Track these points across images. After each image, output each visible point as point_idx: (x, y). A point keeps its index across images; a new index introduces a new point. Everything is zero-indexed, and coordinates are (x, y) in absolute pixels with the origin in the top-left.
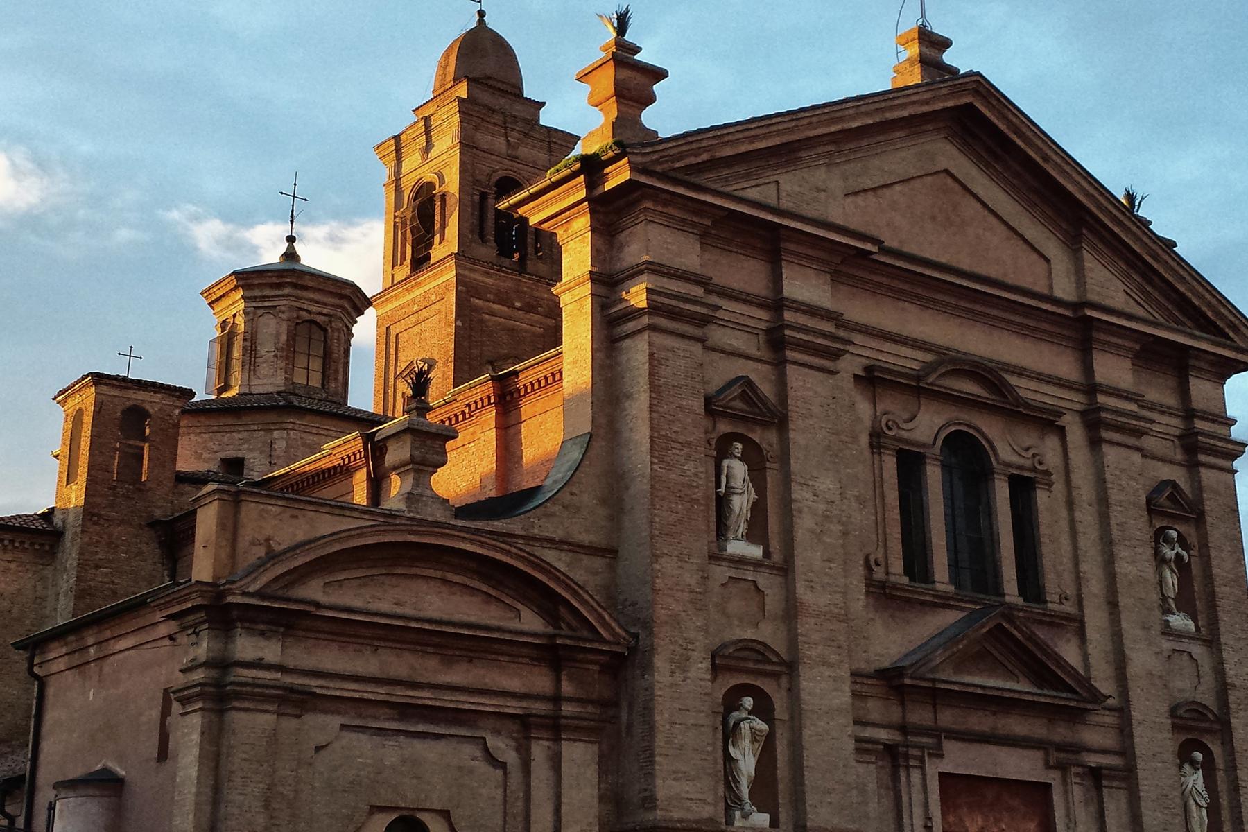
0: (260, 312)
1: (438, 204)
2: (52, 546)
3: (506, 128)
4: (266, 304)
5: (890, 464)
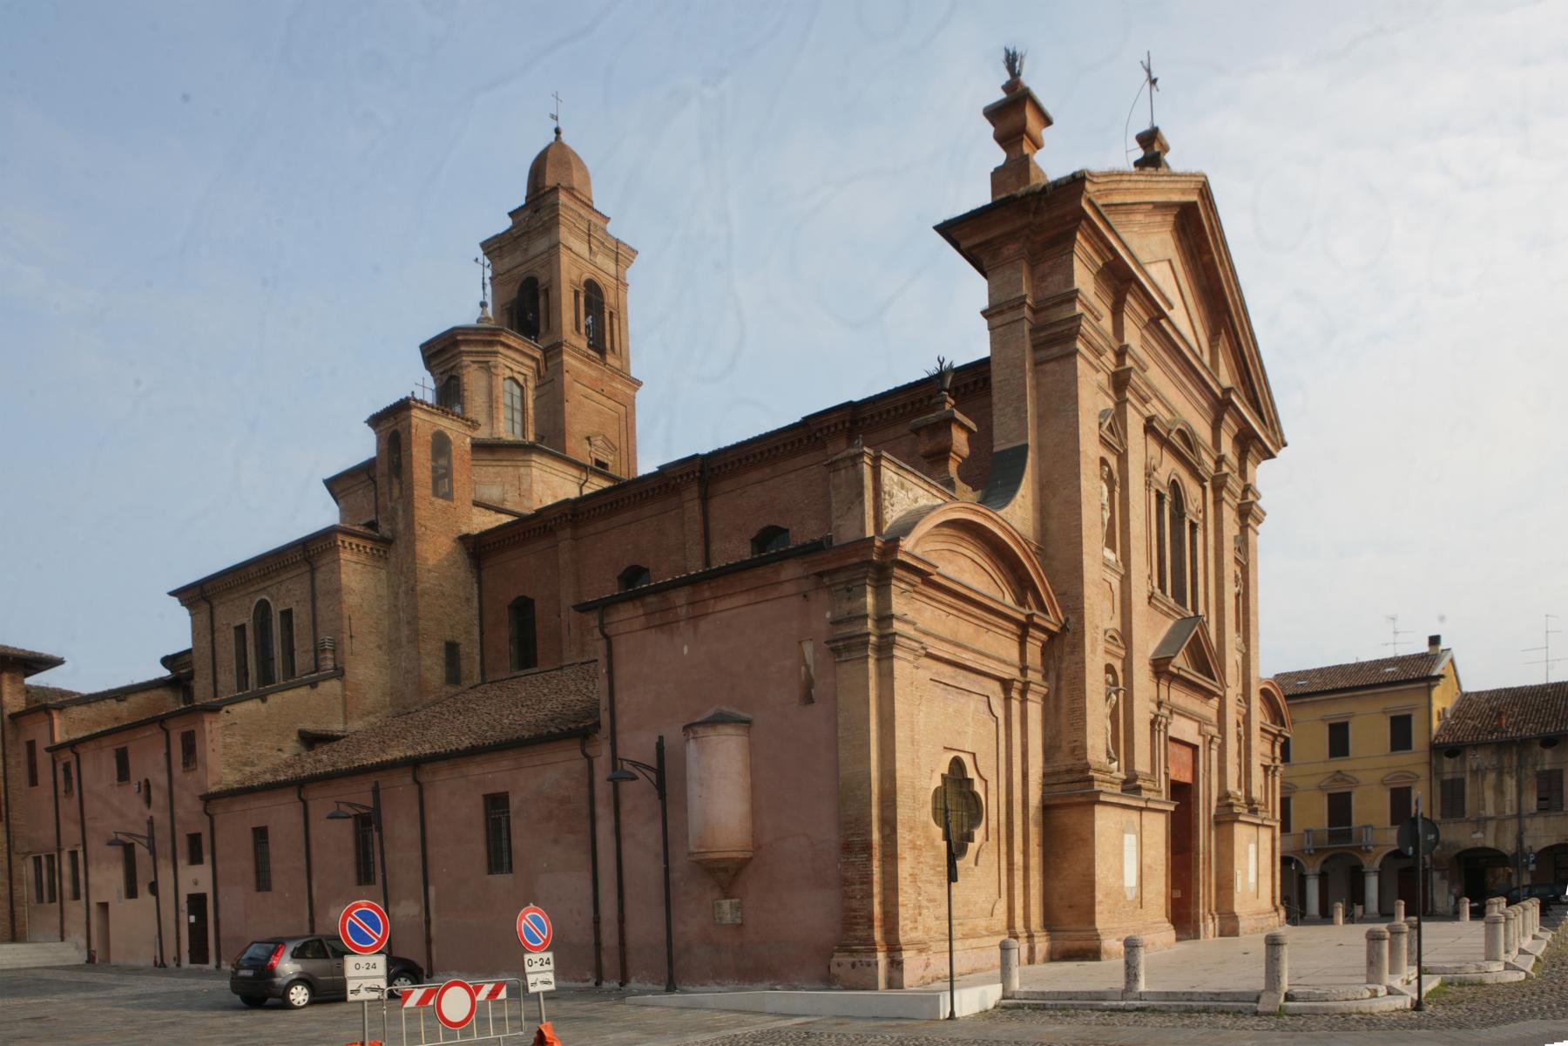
5: (1153, 495)
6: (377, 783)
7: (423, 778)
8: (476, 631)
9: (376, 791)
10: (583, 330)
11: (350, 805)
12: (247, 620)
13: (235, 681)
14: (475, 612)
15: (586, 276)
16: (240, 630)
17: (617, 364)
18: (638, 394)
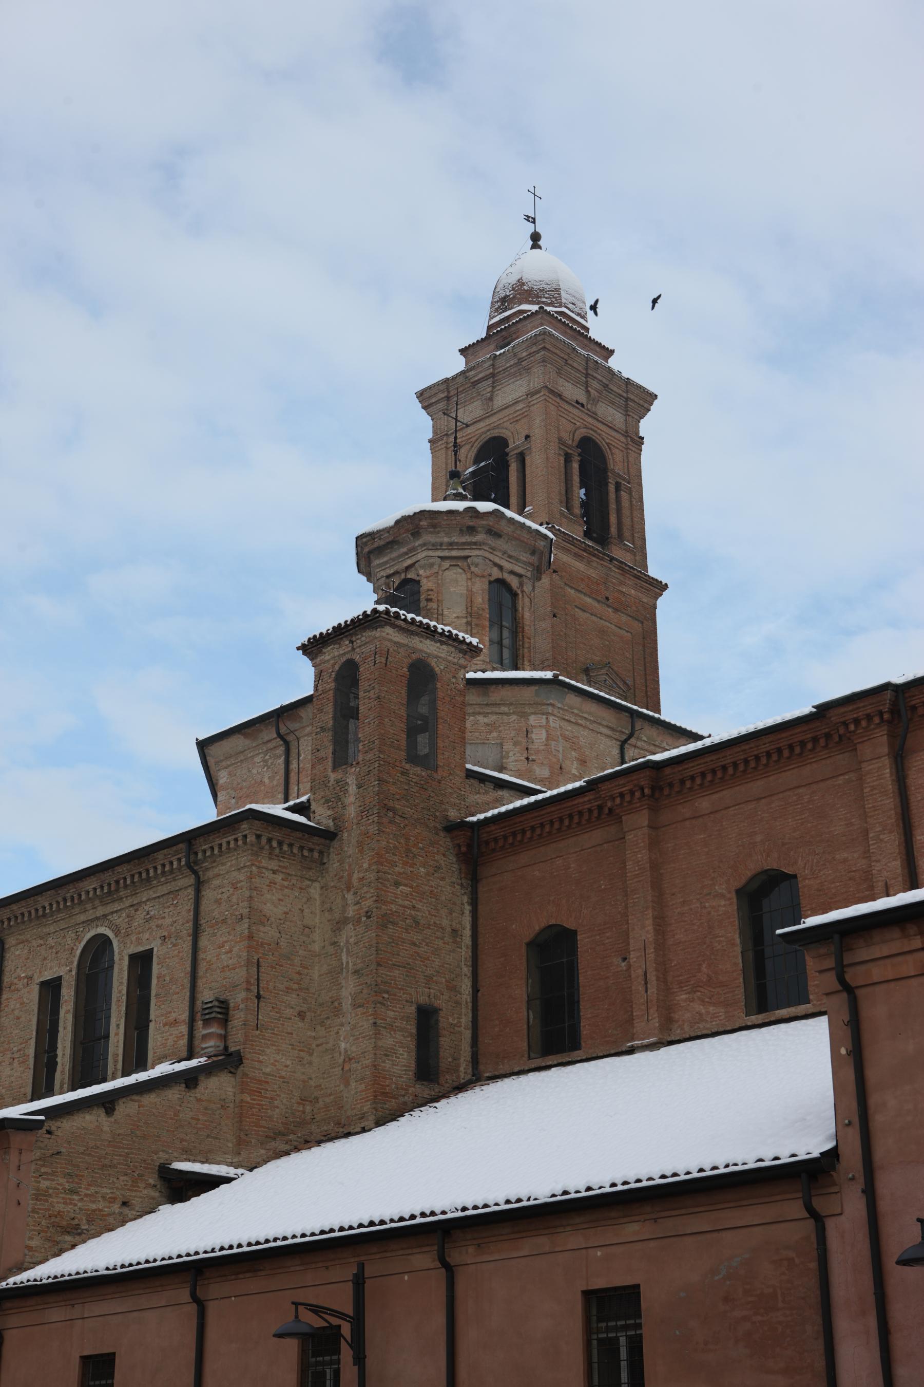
0: (446, 564)
1: (513, 467)
2: (321, 853)
3: (587, 375)
4: (454, 553)
6: (361, 1266)
7: (454, 1257)
8: (466, 986)
9: (359, 1282)
10: (578, 511)
11: (317, 1310)
12: (64, 968)
13: (29, 1076)
14: (465, 952)
15: (582, 432)
16: (51, 988)
17: (627, 559)
18: (660, 602)
